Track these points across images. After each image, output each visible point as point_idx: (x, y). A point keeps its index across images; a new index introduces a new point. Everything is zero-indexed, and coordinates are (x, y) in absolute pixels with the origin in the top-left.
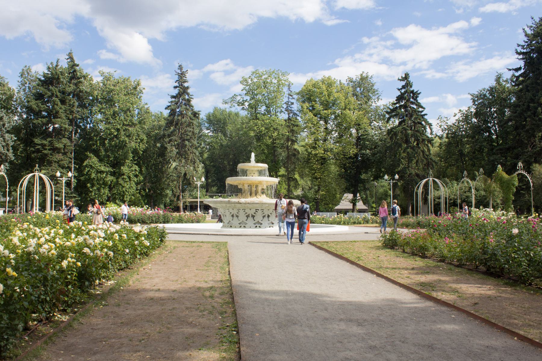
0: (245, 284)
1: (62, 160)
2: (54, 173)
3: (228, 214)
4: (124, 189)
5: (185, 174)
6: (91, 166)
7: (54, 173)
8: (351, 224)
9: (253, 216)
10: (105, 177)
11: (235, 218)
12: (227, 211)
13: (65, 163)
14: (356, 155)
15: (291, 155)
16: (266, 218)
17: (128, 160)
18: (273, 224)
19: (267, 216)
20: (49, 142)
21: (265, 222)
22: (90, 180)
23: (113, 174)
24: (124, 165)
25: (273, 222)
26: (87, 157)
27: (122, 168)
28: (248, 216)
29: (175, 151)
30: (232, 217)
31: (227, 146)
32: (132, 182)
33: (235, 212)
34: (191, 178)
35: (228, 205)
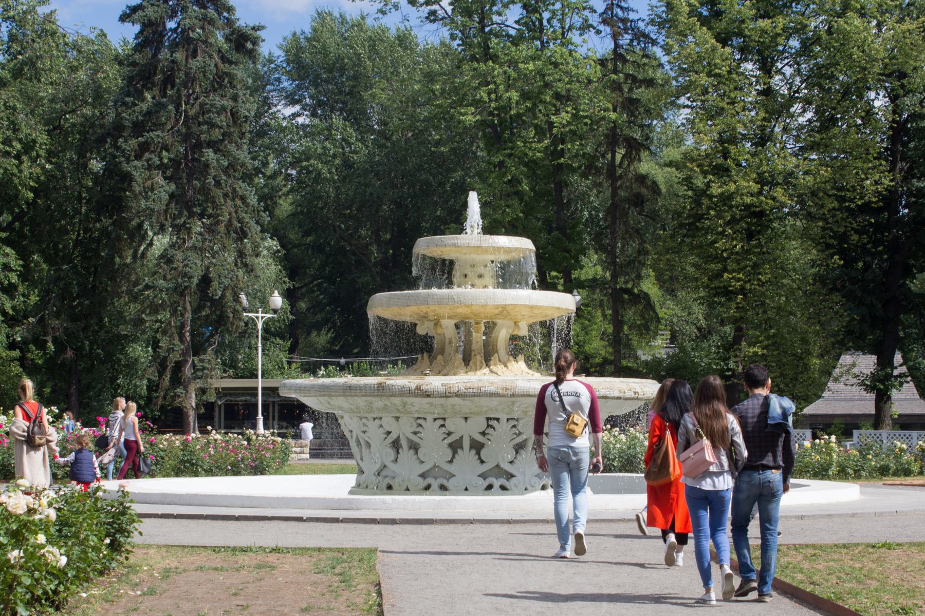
3: (375, 434)
5: (206, 281)
9: (477, 447)
11: (406, 454)
12: (373, 426)
14: (890, 199)
15: (627, 200)
28: (456, 446)
29: (163, 188)
30: (392, 452)
33: (404, 429)
34: (229, 294)
35: (378, 403)
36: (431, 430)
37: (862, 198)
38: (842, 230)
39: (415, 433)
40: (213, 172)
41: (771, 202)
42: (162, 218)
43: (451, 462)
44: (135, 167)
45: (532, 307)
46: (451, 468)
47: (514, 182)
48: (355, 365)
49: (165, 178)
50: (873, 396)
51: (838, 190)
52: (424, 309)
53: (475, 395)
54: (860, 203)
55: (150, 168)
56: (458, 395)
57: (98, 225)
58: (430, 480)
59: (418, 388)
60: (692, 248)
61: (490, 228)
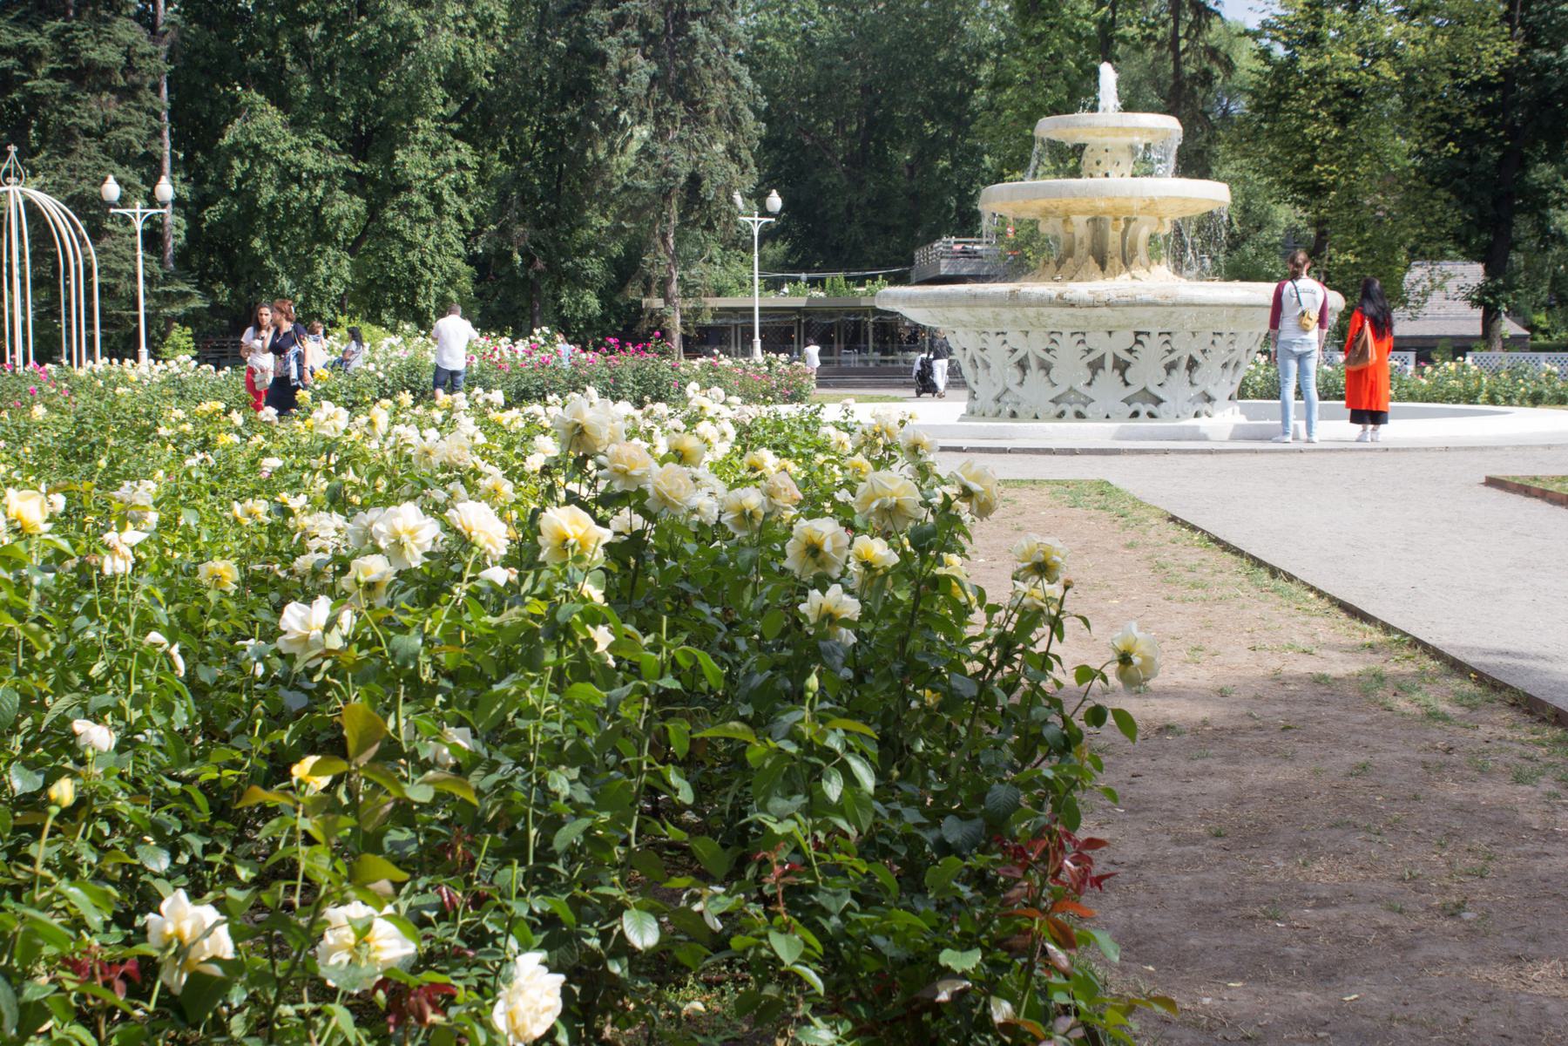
0: (1510, 661)
1: (117, 124)
2: (85, 185)
3: (997, 354)
4: (413, 256)
5: (695, 180)
6: (256, 147)
7: (85, 185)
8: (1521, 404)
9: (1122, 367)
10: (322, 202)
11: (1034, 374)
12: (994, 342)
13: (133, 135)
14: (1510, 74)
15: (1193, 77)
16: (1181, 373)
17: (424, 115)
18: (1209, 399)
19: (1184, 362)
20: (55, 37)
21: (1177, 390)
22: (249, 214)
23: (356, 184)
24: (405, 142)
25: (1212, 392)
26: (235, 109)
27: (400, 155)
28: (1096, 366)
29: (643, 68)
30: (1017, 373)
31: (840, 47)
32: (448, 221)
33: (1034, 346)
34: (722, 196)
35: (1007, 314)
36: (1067, 343)
37: (1477, 72)
38: (1456, 111)
39: (1048, 351)
40: (701, 49)
41: (1373, 78)
42: (643, 104)
43: (1089, 384)
44: (611, 45)
45: (1185, 199)
46: (1090, 392)
47: (1057, 58)
48: (828, 282)
49: (645, 57)
50: (1478, 313)
51: (1455, 62)
52: (1054, 202)
53: (1128, 304)
54: (1476, 78)
55: (627, 44)
56: (1108, 304)
57: (564, 115)
58: (1062, 406)
59: (1060, 296)
60: (1271, 134)
61: (1128, 107)
